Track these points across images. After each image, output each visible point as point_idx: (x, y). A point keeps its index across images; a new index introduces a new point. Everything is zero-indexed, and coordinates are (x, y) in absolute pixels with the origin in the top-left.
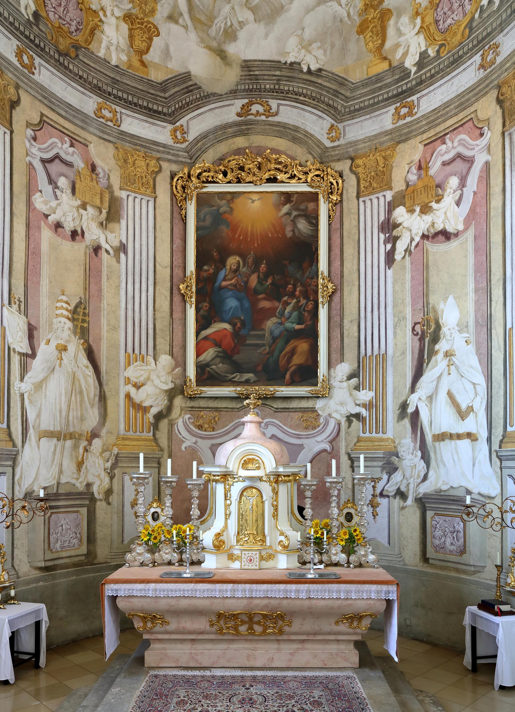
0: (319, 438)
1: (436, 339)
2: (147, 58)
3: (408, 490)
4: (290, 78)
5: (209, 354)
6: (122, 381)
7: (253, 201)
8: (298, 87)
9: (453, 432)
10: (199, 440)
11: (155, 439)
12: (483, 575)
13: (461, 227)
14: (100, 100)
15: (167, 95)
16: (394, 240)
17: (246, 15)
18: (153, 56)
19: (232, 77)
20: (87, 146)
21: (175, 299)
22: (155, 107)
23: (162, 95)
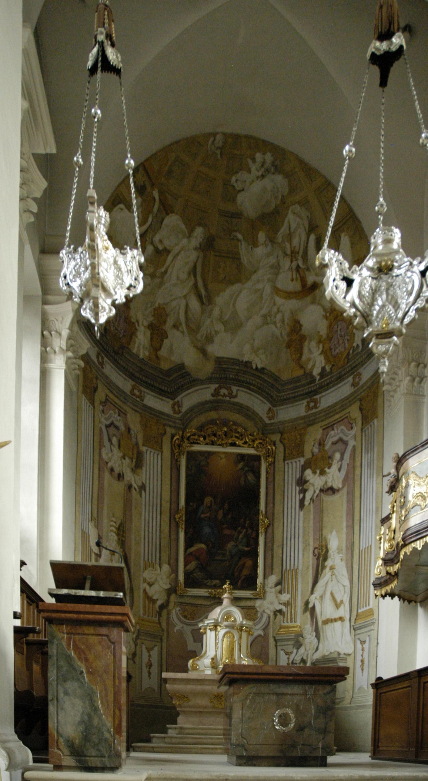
1: (325, 559)
3: (307, 659)
5: (193, 565)
6: (142, 581)
7: (221, 459)
8: (250, 379)
9: (333, 617)
10: (185, 626)
11: (160, 623)
12: (344, 702)
13: (340, 486)
14: (133, 383)
15: (170, 379)
16: (304, 491)
17: (219, 327)
18: (163, 352)
19: (209, 368)
20: (126, 415)
21: (172, 525)
22: (163, 388)
23: (167, 379)
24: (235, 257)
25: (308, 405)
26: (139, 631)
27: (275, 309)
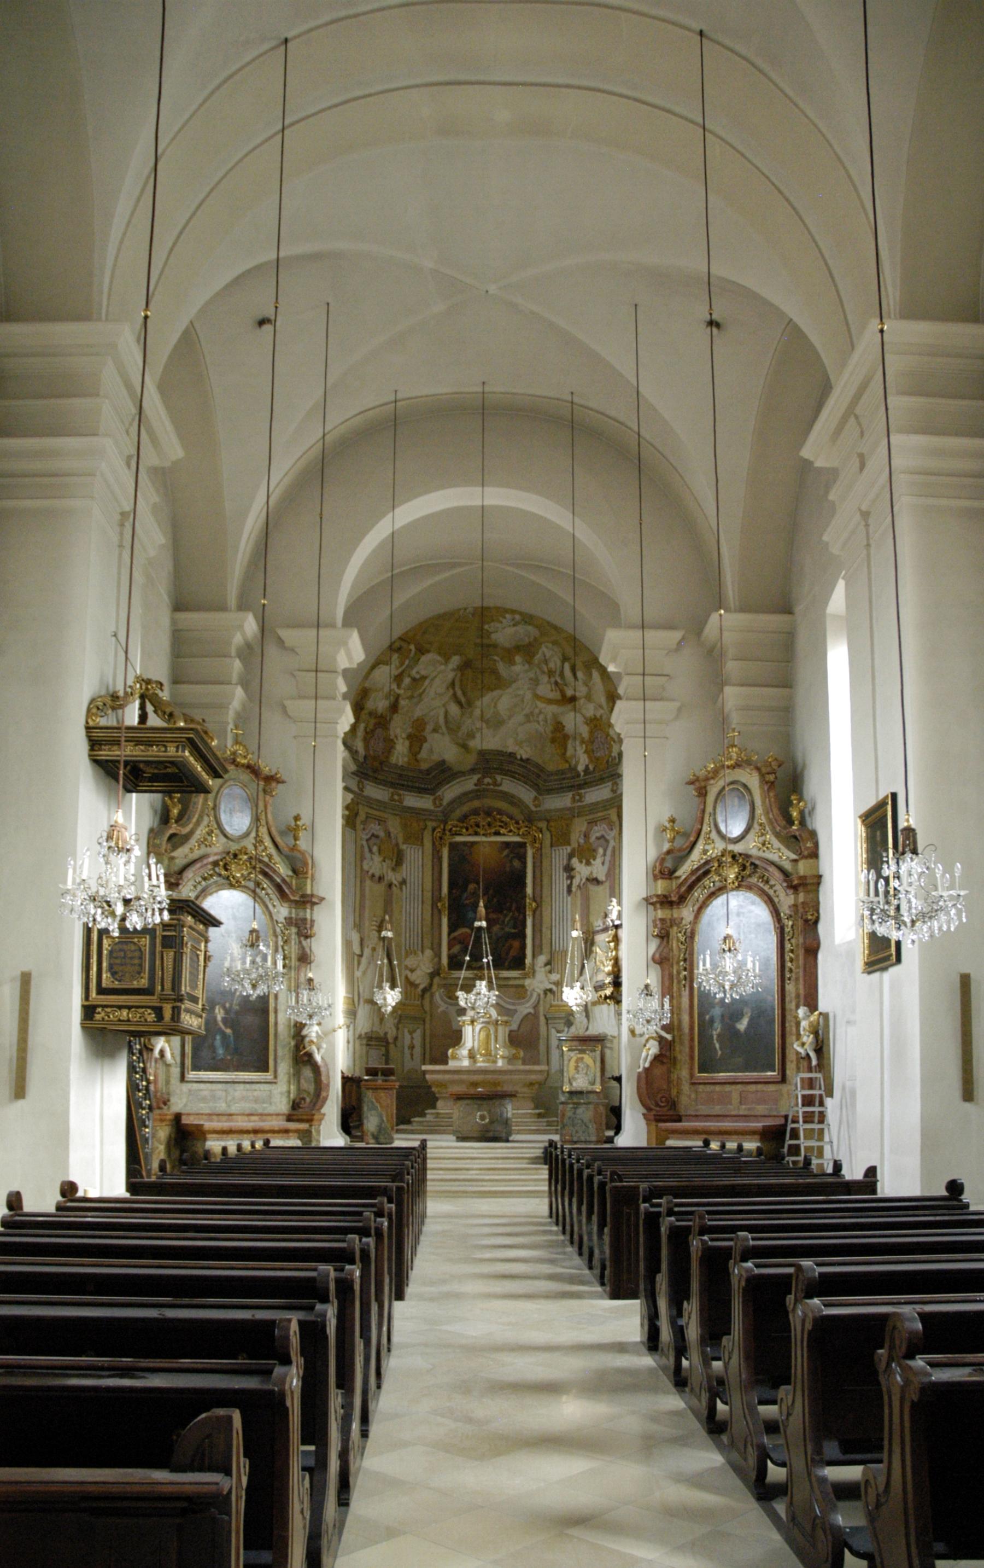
0: (527, 1005)
2: (419, 756)
4: (511, 763)
11: (422, 1006)
16: (571, 878)
18: (423, 754)
19: (471, 760)
24: (494, 672)
25: (573, 798)
26: (400, 1016)
27: (537, 711)
